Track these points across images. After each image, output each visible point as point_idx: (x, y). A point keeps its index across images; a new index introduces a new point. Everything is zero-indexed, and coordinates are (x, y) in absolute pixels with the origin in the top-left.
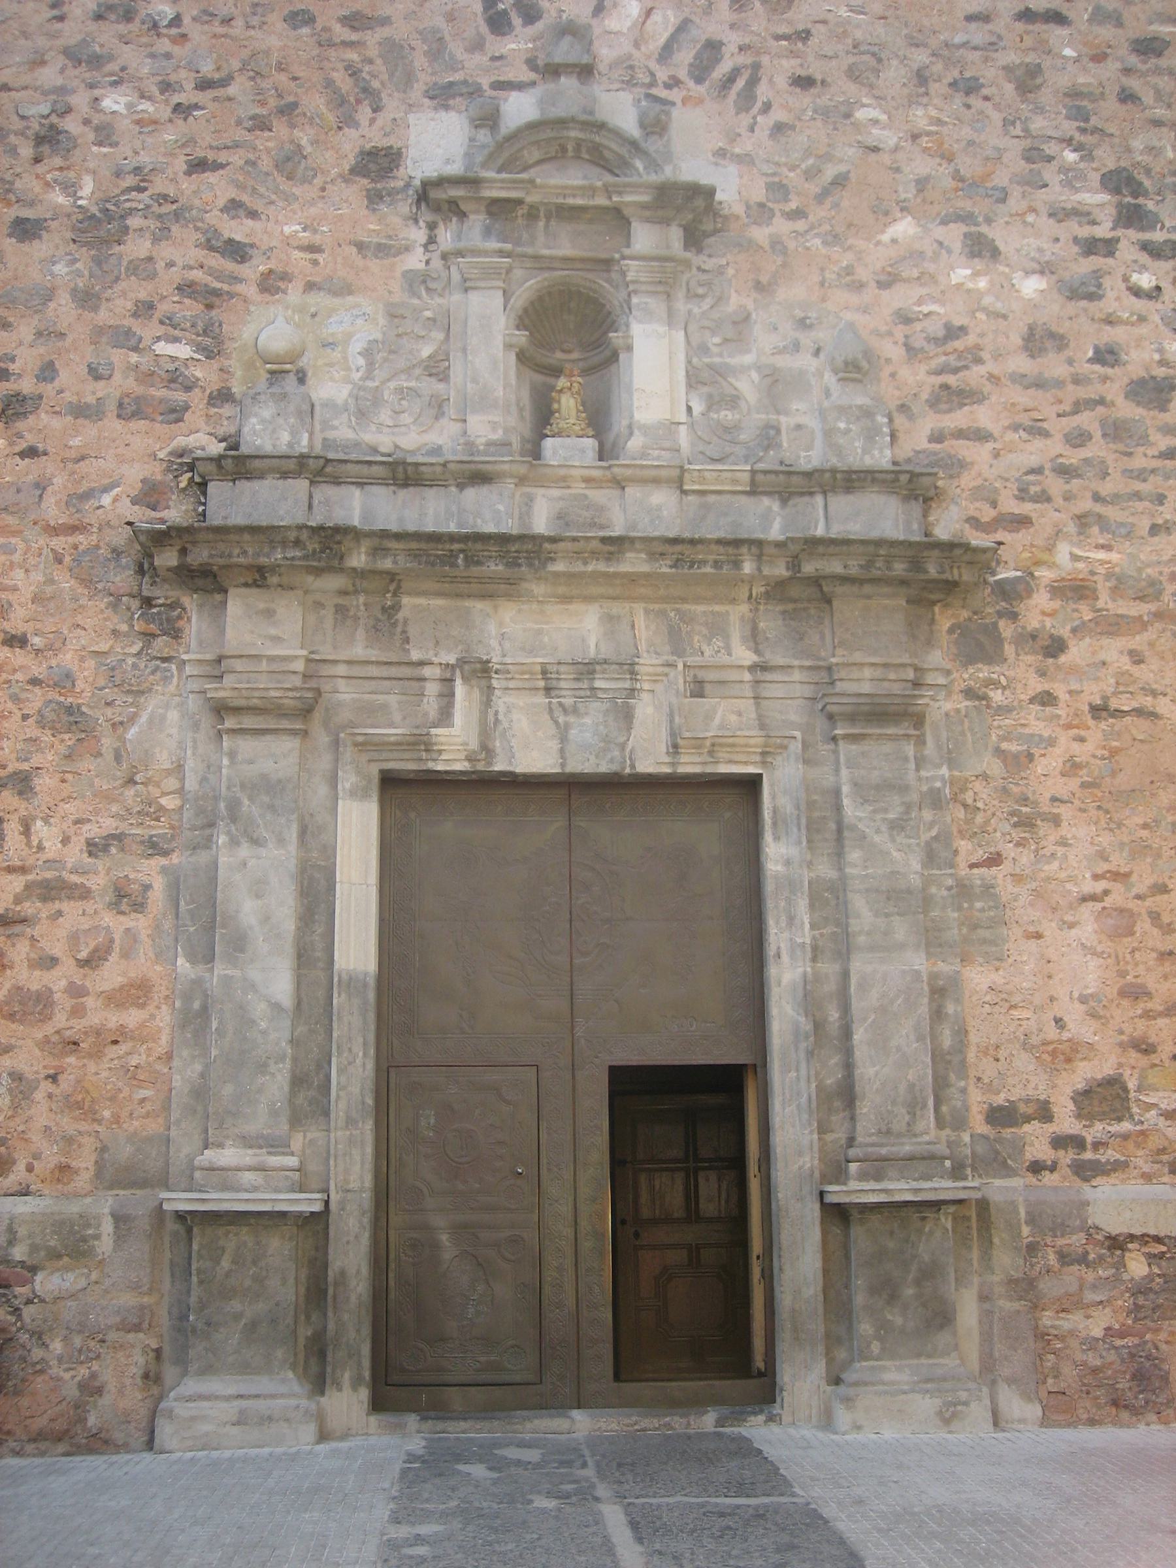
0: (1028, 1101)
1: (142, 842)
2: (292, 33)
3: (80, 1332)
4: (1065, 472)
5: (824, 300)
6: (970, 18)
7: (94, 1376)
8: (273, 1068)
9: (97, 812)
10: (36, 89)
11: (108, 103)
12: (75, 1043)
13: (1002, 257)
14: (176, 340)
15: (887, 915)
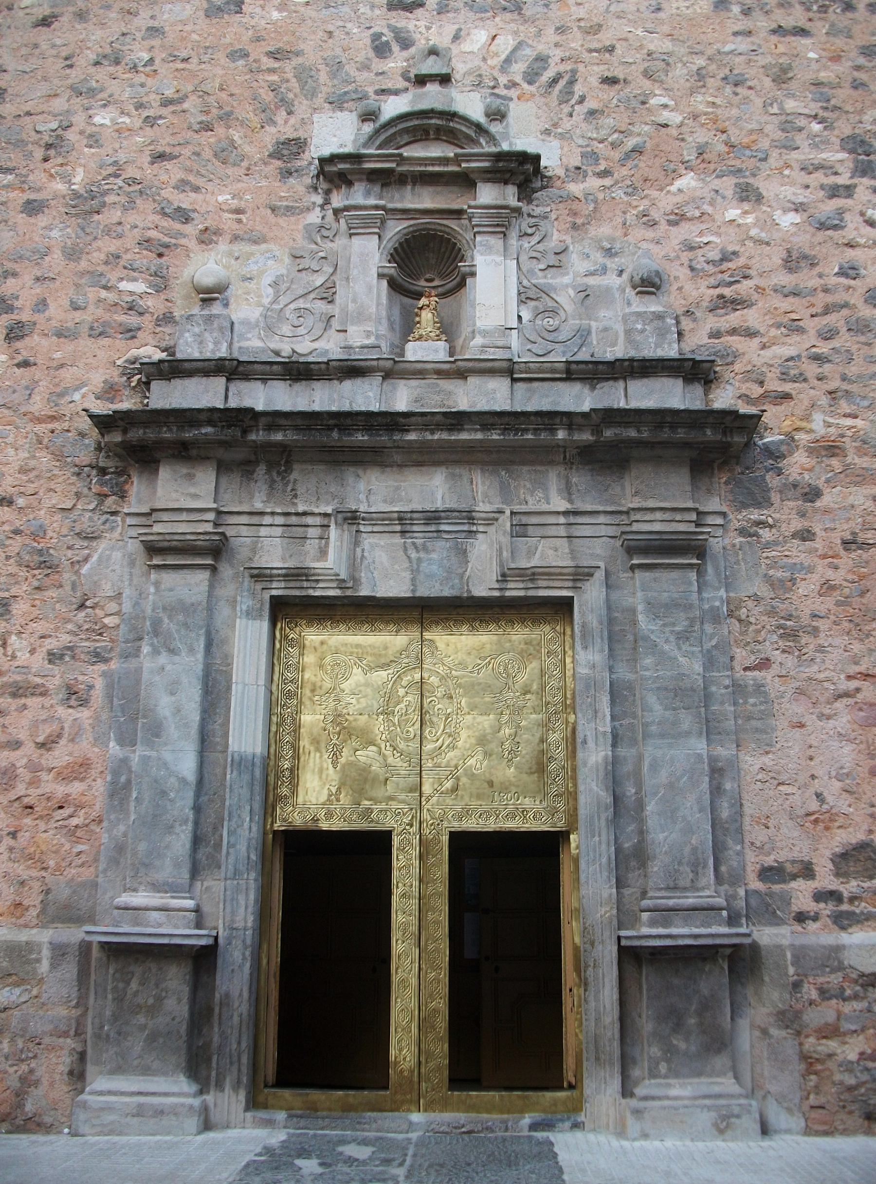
0: (793, 862)
1: (89, 652)
2: (232, 65)
3: (22, 1036)
4: (817, 358)
5: (626, 235)
6: (736, 34)
7: (32, 1071)
8: (178, 829)
9: (57, 629)
10: (49, 113)
11: (97, 120)
12: (31, 808)
13: (764, 200)
14: (135, 280)
15: (674, 709)
